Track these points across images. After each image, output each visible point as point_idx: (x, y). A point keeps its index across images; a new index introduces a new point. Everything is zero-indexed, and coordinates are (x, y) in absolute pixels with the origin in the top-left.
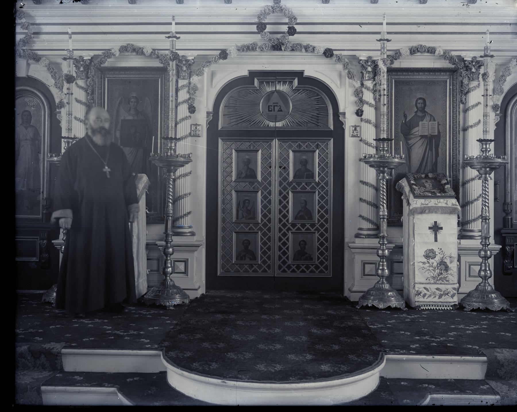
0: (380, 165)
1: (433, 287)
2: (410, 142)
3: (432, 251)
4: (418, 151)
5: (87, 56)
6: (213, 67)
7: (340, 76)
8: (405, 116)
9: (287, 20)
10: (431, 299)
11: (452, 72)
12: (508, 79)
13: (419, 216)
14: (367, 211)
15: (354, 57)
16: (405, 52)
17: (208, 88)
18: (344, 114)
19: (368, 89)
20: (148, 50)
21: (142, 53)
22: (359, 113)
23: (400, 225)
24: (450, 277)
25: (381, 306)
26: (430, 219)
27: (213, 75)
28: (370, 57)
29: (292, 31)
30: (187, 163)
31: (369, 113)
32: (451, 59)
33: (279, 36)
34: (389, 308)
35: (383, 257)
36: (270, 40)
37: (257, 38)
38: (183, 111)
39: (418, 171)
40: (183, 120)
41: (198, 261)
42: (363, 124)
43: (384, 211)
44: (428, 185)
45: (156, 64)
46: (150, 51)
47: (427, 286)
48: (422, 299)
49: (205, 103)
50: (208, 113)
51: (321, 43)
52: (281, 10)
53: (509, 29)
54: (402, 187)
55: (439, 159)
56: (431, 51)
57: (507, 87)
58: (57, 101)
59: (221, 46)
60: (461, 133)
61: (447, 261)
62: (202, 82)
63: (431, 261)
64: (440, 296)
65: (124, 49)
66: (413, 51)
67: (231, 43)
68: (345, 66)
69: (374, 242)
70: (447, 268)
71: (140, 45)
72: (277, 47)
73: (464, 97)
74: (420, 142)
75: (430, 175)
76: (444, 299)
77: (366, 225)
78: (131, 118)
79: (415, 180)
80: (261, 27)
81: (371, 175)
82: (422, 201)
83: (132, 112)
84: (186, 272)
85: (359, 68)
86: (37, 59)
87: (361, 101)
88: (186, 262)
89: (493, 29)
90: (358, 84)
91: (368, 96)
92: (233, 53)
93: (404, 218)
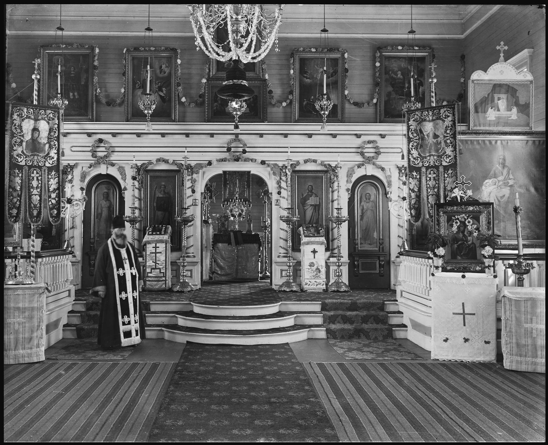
0: (287, 221)
1: (313, 281)
2: (305, 208)
3: (313, 263)
4: (309, 212)
5: (139, 164)
6: (204, 169)
7: (269, 174)
8: (303, 195)
9: (242, 146)
10: (312, 287)
11: (326, 172)
12: (354, 175)
13: (307, 246)
14: (282, 243)
15: (276, 164)
16: (302, 162)
17: (201, 182)
18: (271, 193)
19: (283, 181)
20: (171, 161)
21: (168, 162)
22: (279, 193)
23: (299, 251)
24: (321, 276)
25: (288, 290)
26: (311, 247)
27: (204, 173)
28: (284, 165)
29: (244, 152)
30: (192, 220)
31: (284, 193)
32: (325, 165)
33: (238, 154)
34: (292, 291)
35: (290, 266)
36: (233, 156)
37: (226, 155)
38: (189, 192)
39: (309, 223)
40: (189, 197)
41: (197, 270)
42: (281, 199)
43: (290, 243)
44: (312, 230)
45: (175, 168)
46: (172, 162)
47: (310, 280)
48: (308, 287)
49: (200, 188)
50: (202, 193)
51: (260, 157)
52: (239, 140)
53: (117, 149)
54: (300, 231)
55: (320, 216)
56: (315, 161)
57: (354, 179)
58: (123, 187)
59: (209, 159)
60: (330, 203)
61: (320, 268)
62: (198, 177)
63: (312, 268)
64: (317, 285)
65: (158, 160)
66: (306, 161)
67: (213, 157)
68: (272, 169)
69: (286, 260)
70: (320, 271)
71: (167, 158)
72: (237, 160)
73: (332, 185)
74: (310, 208)
75: (314, 225)
76: (319, 286)
77: (282, 251)
78: (161, 196)
79: (306, 228)
80: (229, 150)
81: (284, 225)
82: (308, 238)
83: (162, 193)
84: (191, 277)
85: (279, 170)
86: (113, 165)
87: (280, 187)
88: (191, 271)
89: (189, 149)
90: (278, 178)
91: (283, 184)
92: (215, 163)
93: (302, 248)
